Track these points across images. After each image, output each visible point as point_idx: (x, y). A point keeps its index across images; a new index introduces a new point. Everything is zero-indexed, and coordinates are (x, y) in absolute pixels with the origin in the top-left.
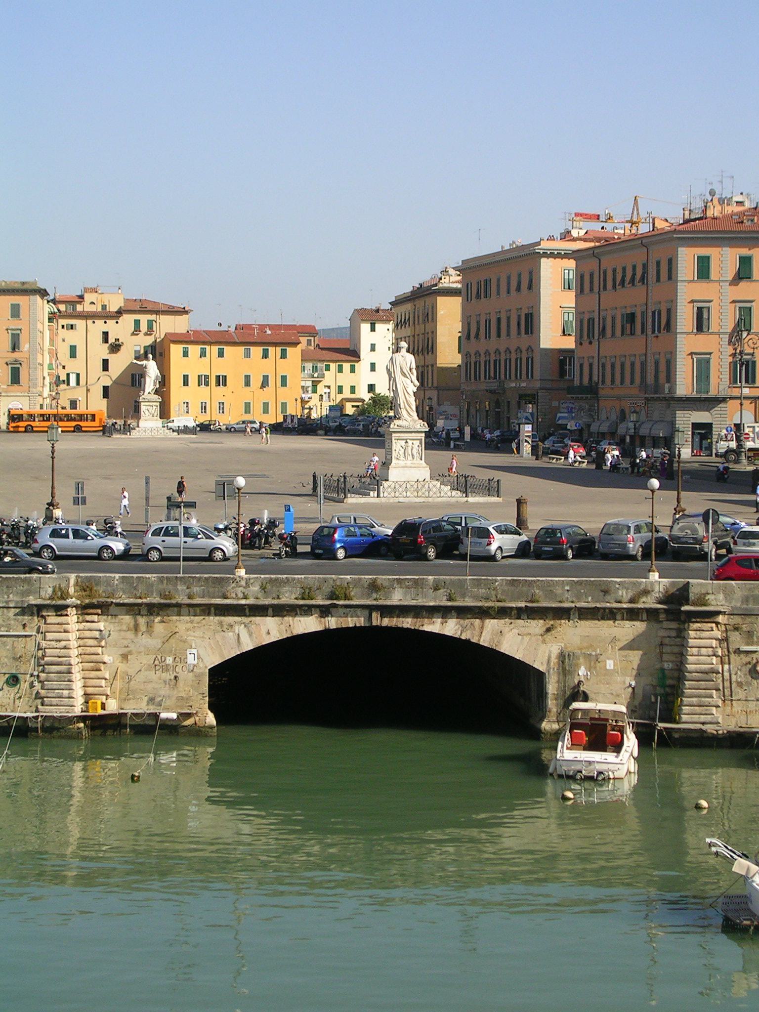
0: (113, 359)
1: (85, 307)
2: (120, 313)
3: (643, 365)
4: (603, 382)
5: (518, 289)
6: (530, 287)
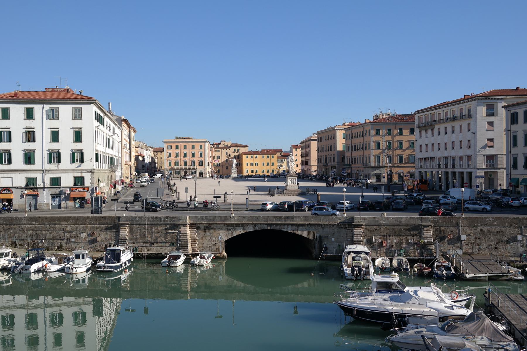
2: (230, 147)
3: (363, 158)
5: (331, 139)
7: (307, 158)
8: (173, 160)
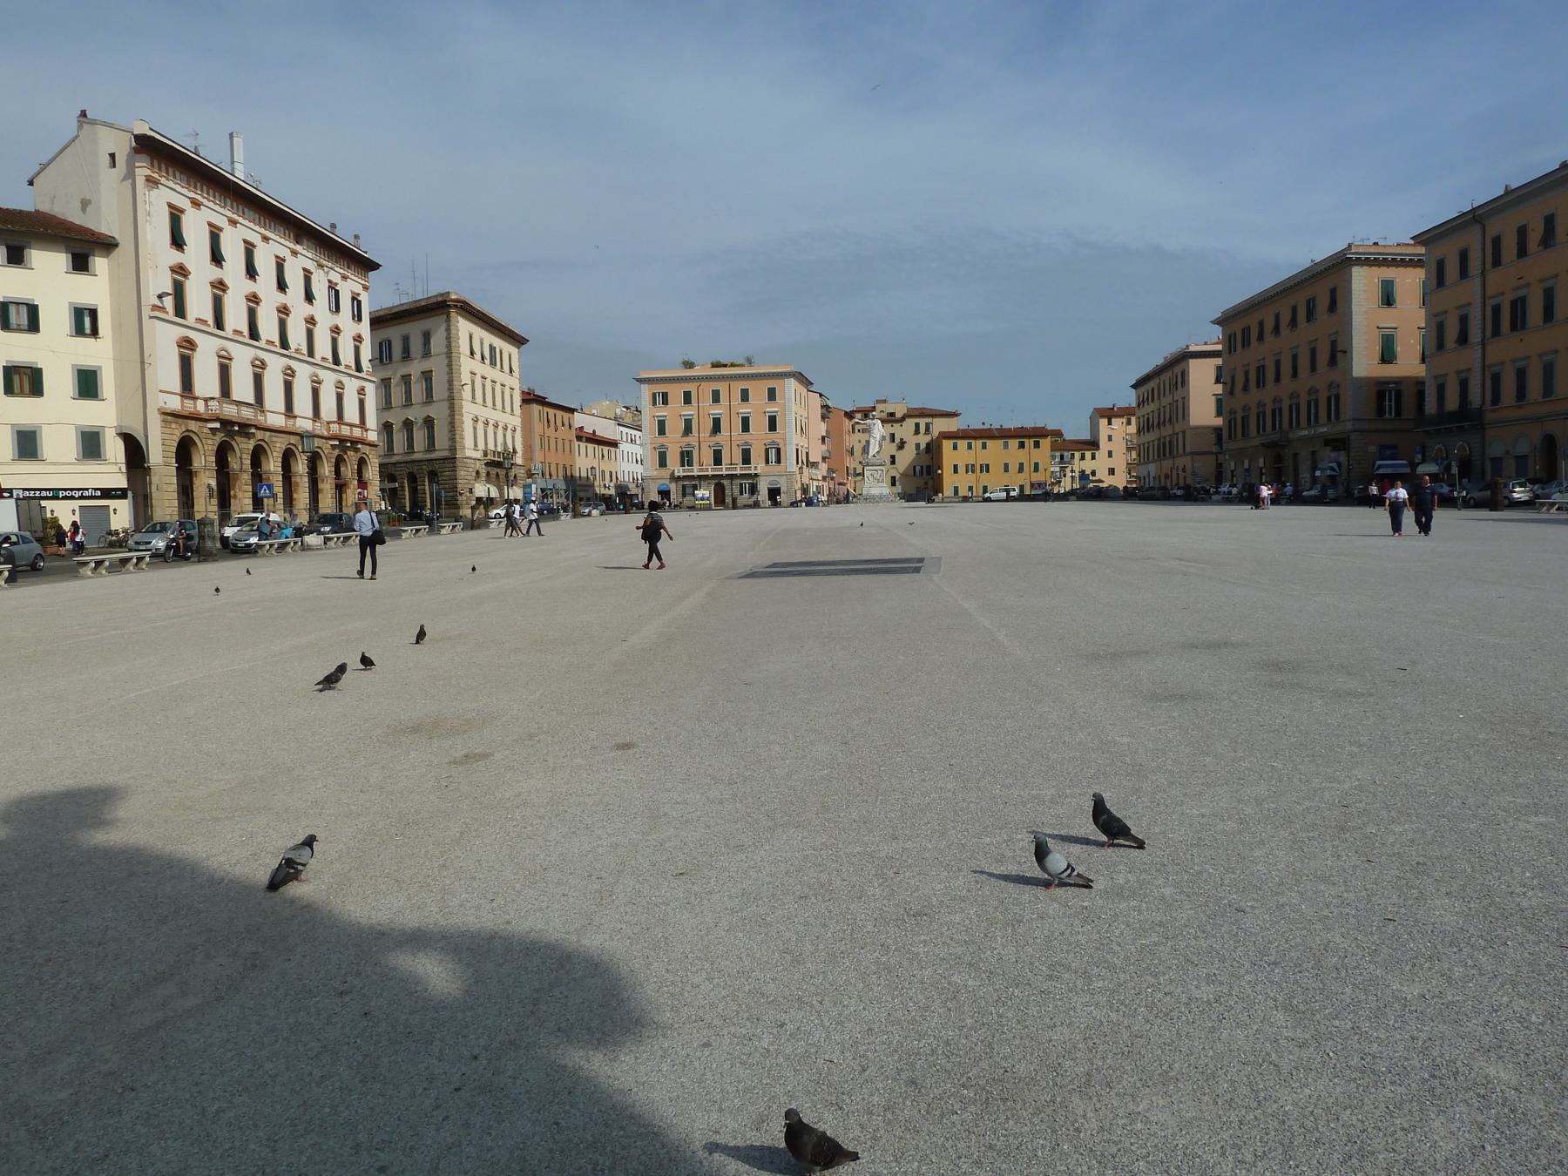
0: (900, 456)
2: (903, 419)
4: (1496, 399)
7: (1167, 431)
8: (674, 442)
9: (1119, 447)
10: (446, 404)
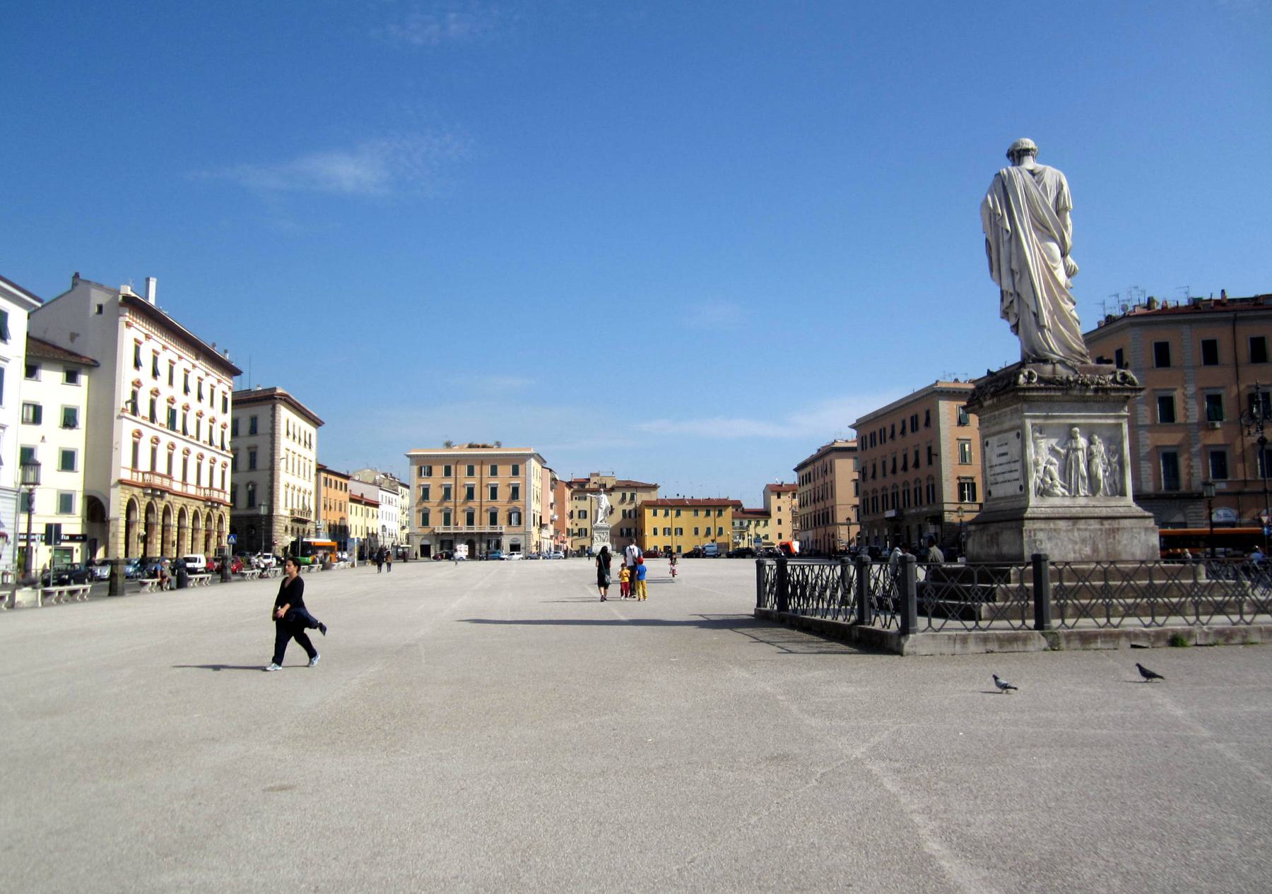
1: (591, 486)
2: (612, 489)
6: (927, 424)
7: (820, 505)
9: (787, 517)
10: (268, 473)
